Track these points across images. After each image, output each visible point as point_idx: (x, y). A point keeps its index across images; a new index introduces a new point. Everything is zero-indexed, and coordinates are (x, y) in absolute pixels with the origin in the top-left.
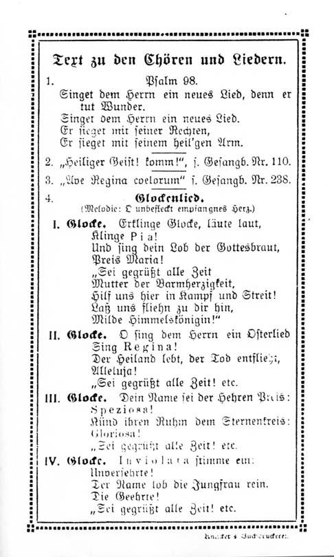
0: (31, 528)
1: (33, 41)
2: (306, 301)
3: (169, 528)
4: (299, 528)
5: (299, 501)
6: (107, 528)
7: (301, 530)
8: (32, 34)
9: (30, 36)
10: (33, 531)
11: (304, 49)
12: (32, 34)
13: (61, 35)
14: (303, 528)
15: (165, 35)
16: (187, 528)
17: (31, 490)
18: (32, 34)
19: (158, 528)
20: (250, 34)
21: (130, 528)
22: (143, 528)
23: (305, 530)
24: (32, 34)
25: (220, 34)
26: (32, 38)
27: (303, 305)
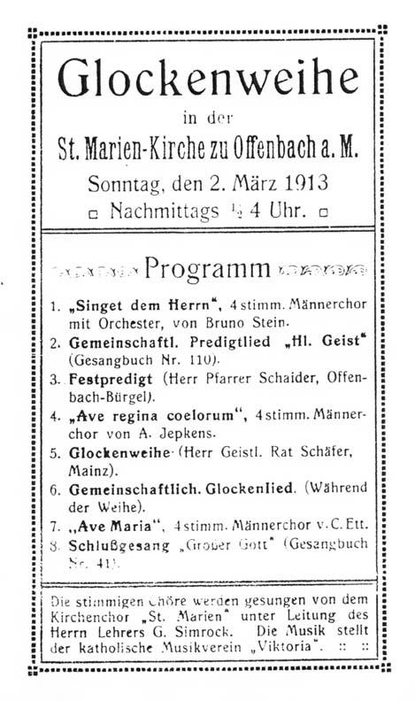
0: (386, 668)
1: (34, 43)
2: (31, 471)
3: (210, 32)
4: (38, 33)
5: (37, 474)
6: (383, 381)
7: (30, 668)
8: (33, 33)
9: (30, 36)
10: (389, 665)
11: (33, 651)
12: (32, 33)
13: (34, 333)
14: (386, 668)
15: (35, 590)
16: (159, 33)
17: (33, 298)
18: (33, 33)
19: (384, 454)
20: (34, 396)
21: (86, 33)
22: (384, 543)
23: (30, 30)
24: (32, 33)
25: (33, 448)
26: (33, 39)
27: (34, 252)
